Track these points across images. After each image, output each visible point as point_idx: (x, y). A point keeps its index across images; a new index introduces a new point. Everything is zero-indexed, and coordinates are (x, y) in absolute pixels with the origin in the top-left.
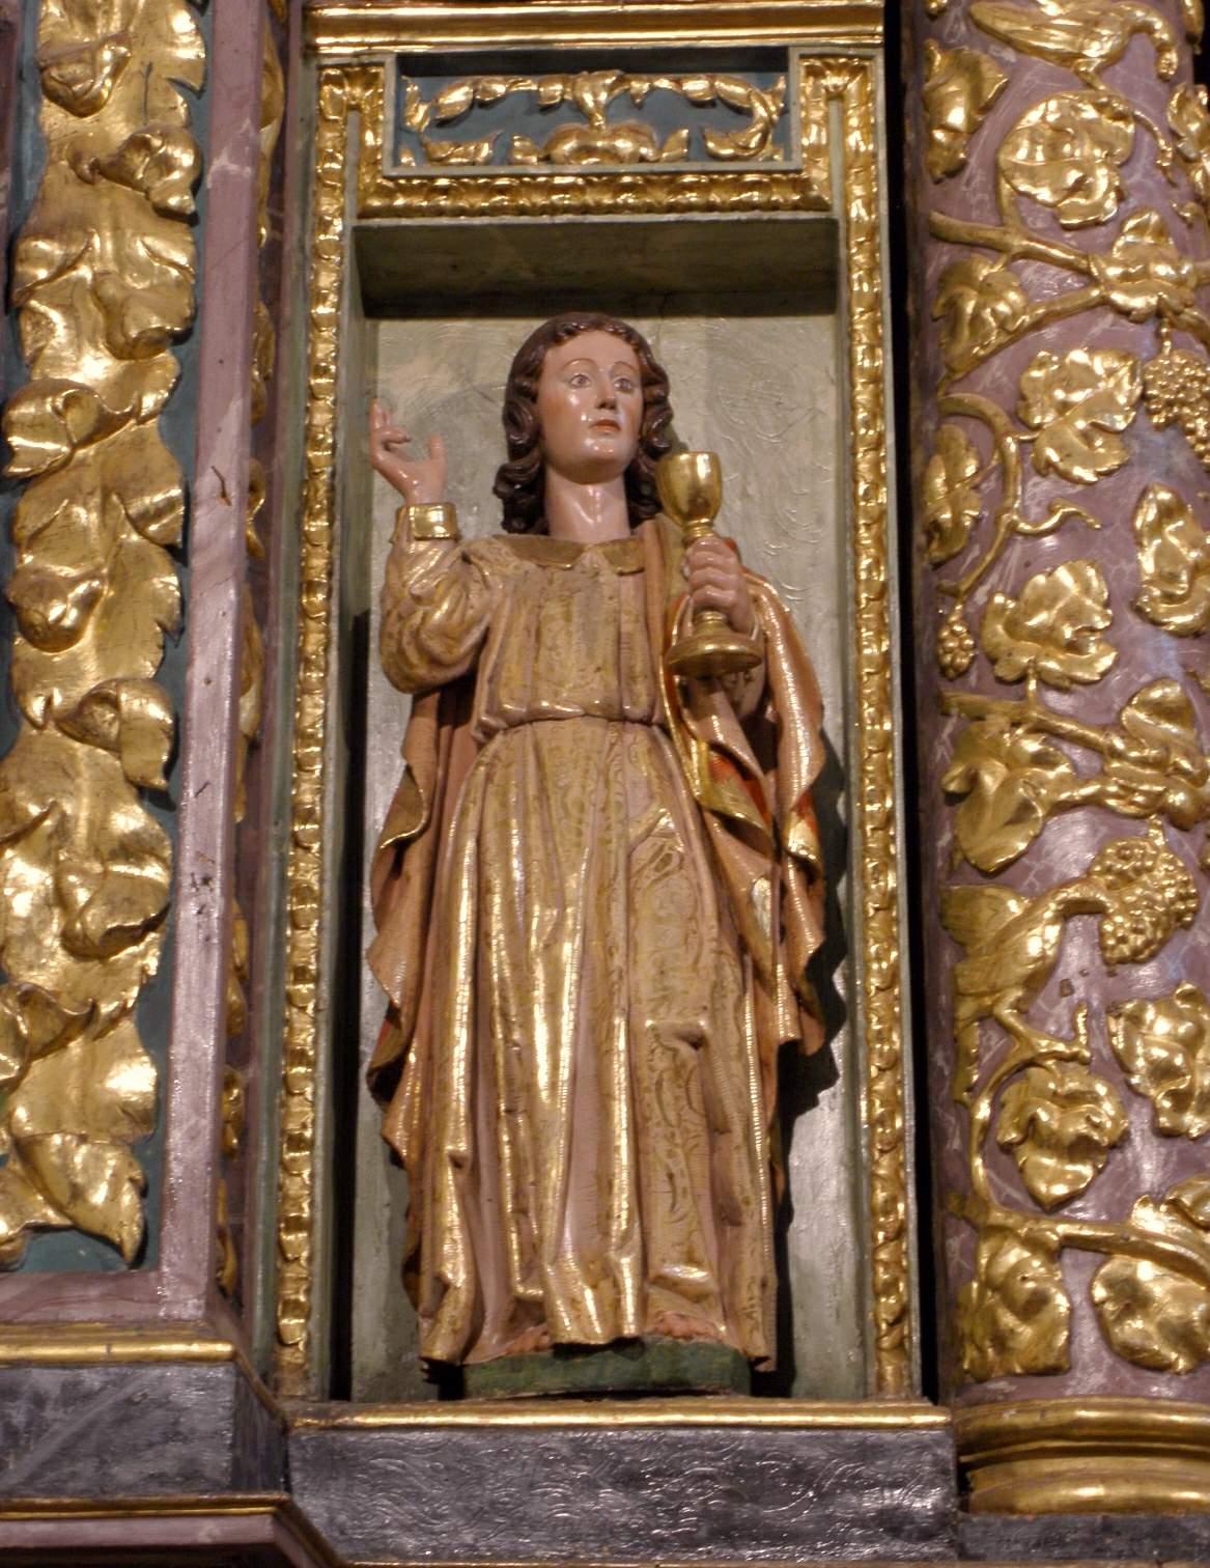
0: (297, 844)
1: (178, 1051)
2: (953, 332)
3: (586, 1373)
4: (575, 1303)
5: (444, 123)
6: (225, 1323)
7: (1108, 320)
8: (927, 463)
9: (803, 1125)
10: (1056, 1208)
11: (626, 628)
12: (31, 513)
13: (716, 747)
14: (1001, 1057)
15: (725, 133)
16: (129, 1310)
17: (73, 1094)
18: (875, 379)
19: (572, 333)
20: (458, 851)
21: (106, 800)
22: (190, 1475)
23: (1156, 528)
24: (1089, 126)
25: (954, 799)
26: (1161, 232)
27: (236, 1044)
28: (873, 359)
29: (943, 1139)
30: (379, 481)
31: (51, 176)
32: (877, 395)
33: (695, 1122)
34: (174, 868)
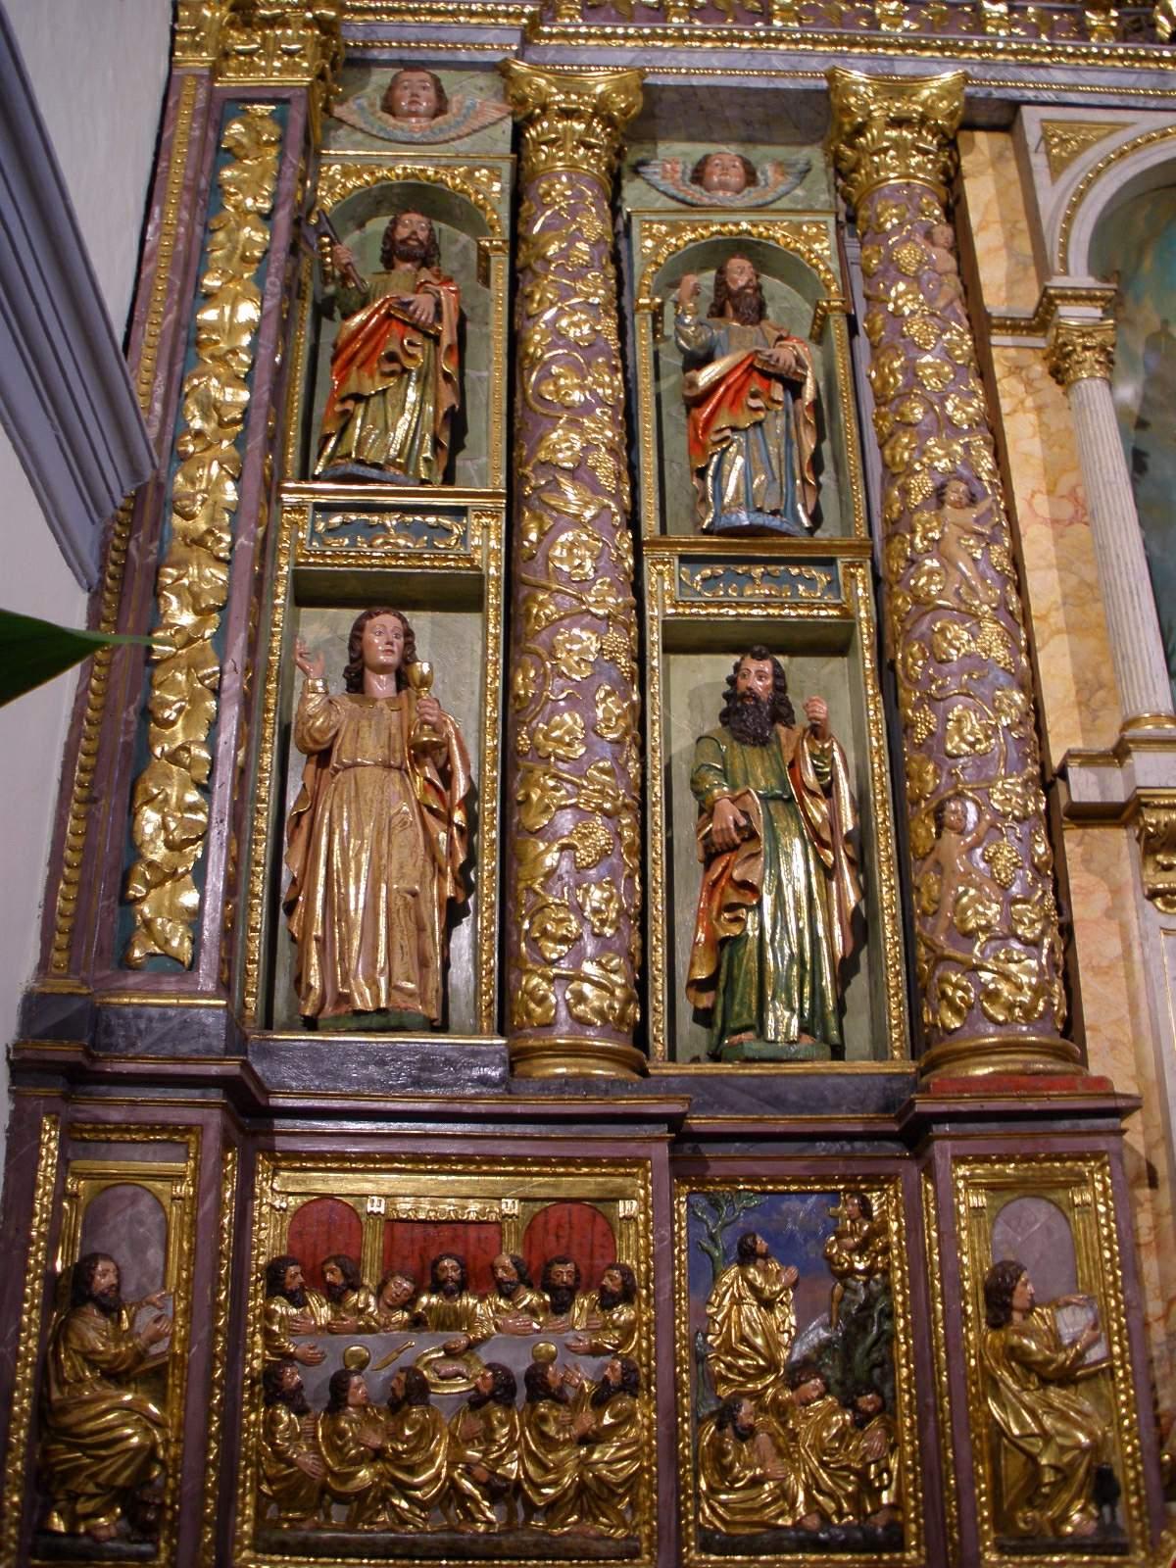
0: (258, 812)
1: (209, 887)
2: (528, 621)
3: (366, 1022)
4: (362, 995)
5: (331, 531)
6: (223, 994)
7: (589, 618)
8: (516, 670)
9: (455, 932)
10: (552, 963)
11: (394, 731)
12: (159, 675)
13: (426, 779)
14: (532, 906)
15: (441, 539)
16: (186, 987)
17: (167, 903)
18: (496, 637)
19: (377, 614)
20: (323, 816)
21: (184, 788)
22: (209, 1050)
23: (604, 700)
24: (584, 543)
25: (520, 803)
26: (610, 585)
27: (232, 888)
28: (495, 629)
29: (510, 935)
30: (298, 671)
31: (175, 543)
32: (497, 644)
33: (412, 926)
34: (209, 816)
